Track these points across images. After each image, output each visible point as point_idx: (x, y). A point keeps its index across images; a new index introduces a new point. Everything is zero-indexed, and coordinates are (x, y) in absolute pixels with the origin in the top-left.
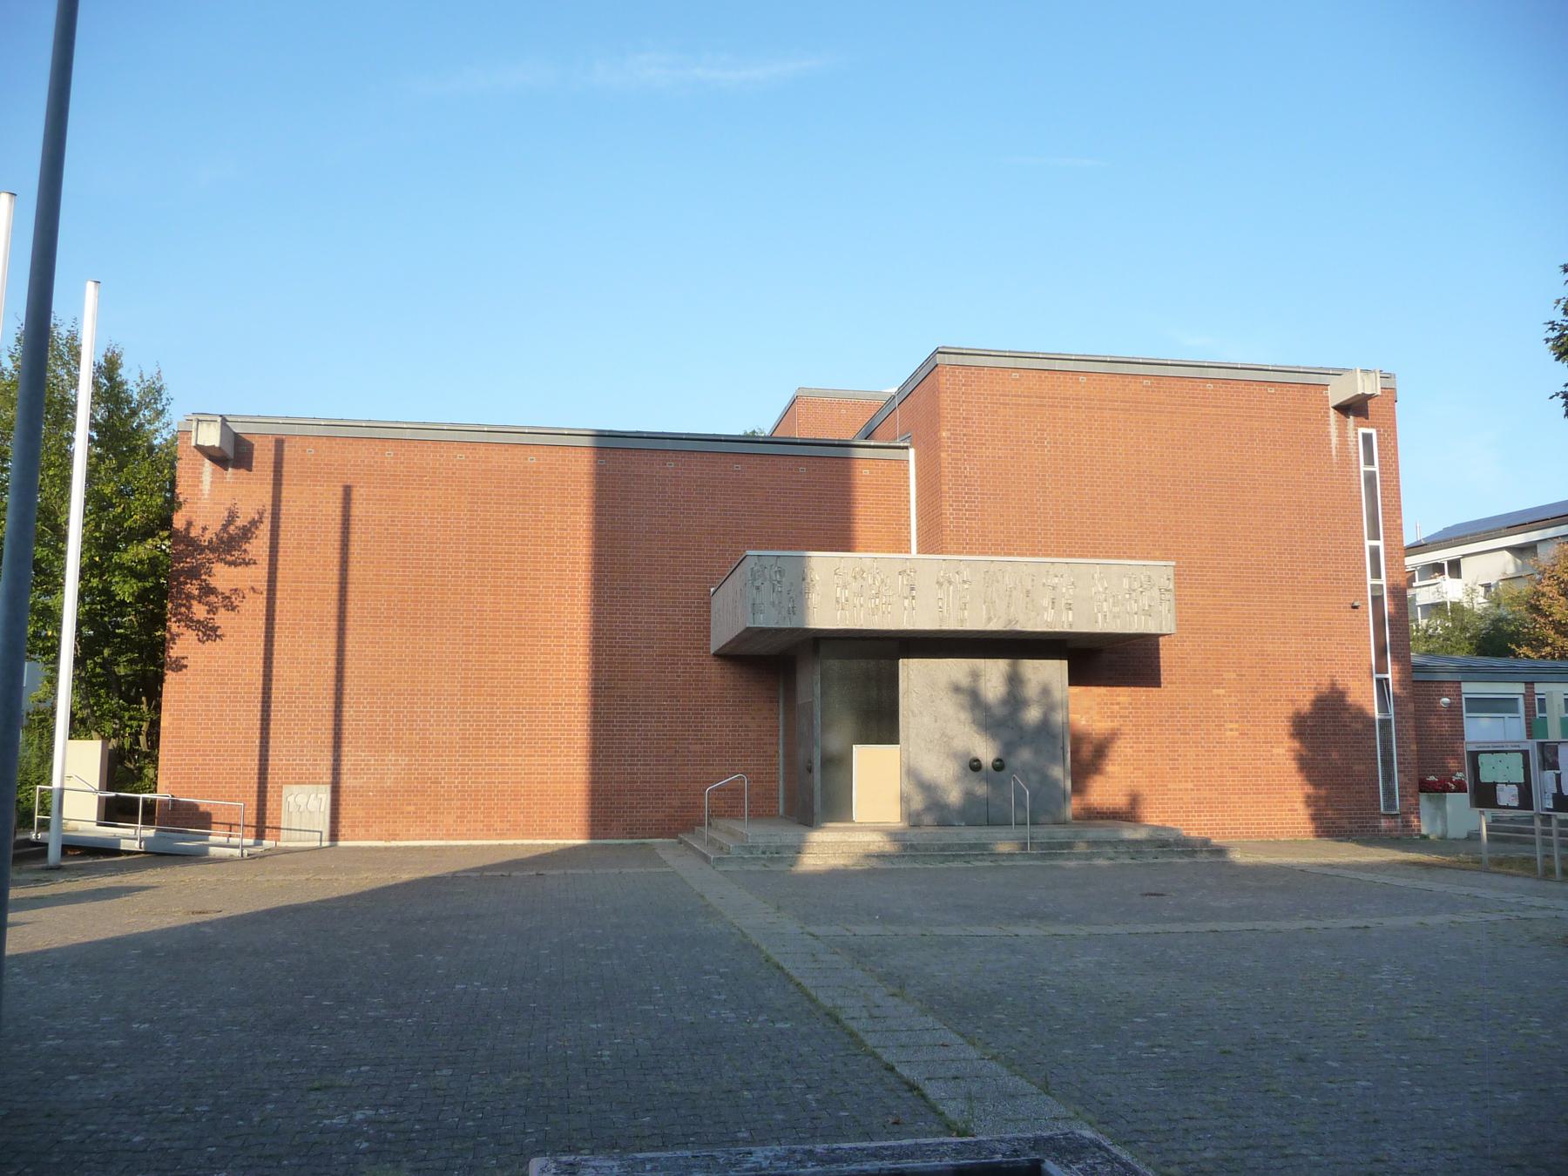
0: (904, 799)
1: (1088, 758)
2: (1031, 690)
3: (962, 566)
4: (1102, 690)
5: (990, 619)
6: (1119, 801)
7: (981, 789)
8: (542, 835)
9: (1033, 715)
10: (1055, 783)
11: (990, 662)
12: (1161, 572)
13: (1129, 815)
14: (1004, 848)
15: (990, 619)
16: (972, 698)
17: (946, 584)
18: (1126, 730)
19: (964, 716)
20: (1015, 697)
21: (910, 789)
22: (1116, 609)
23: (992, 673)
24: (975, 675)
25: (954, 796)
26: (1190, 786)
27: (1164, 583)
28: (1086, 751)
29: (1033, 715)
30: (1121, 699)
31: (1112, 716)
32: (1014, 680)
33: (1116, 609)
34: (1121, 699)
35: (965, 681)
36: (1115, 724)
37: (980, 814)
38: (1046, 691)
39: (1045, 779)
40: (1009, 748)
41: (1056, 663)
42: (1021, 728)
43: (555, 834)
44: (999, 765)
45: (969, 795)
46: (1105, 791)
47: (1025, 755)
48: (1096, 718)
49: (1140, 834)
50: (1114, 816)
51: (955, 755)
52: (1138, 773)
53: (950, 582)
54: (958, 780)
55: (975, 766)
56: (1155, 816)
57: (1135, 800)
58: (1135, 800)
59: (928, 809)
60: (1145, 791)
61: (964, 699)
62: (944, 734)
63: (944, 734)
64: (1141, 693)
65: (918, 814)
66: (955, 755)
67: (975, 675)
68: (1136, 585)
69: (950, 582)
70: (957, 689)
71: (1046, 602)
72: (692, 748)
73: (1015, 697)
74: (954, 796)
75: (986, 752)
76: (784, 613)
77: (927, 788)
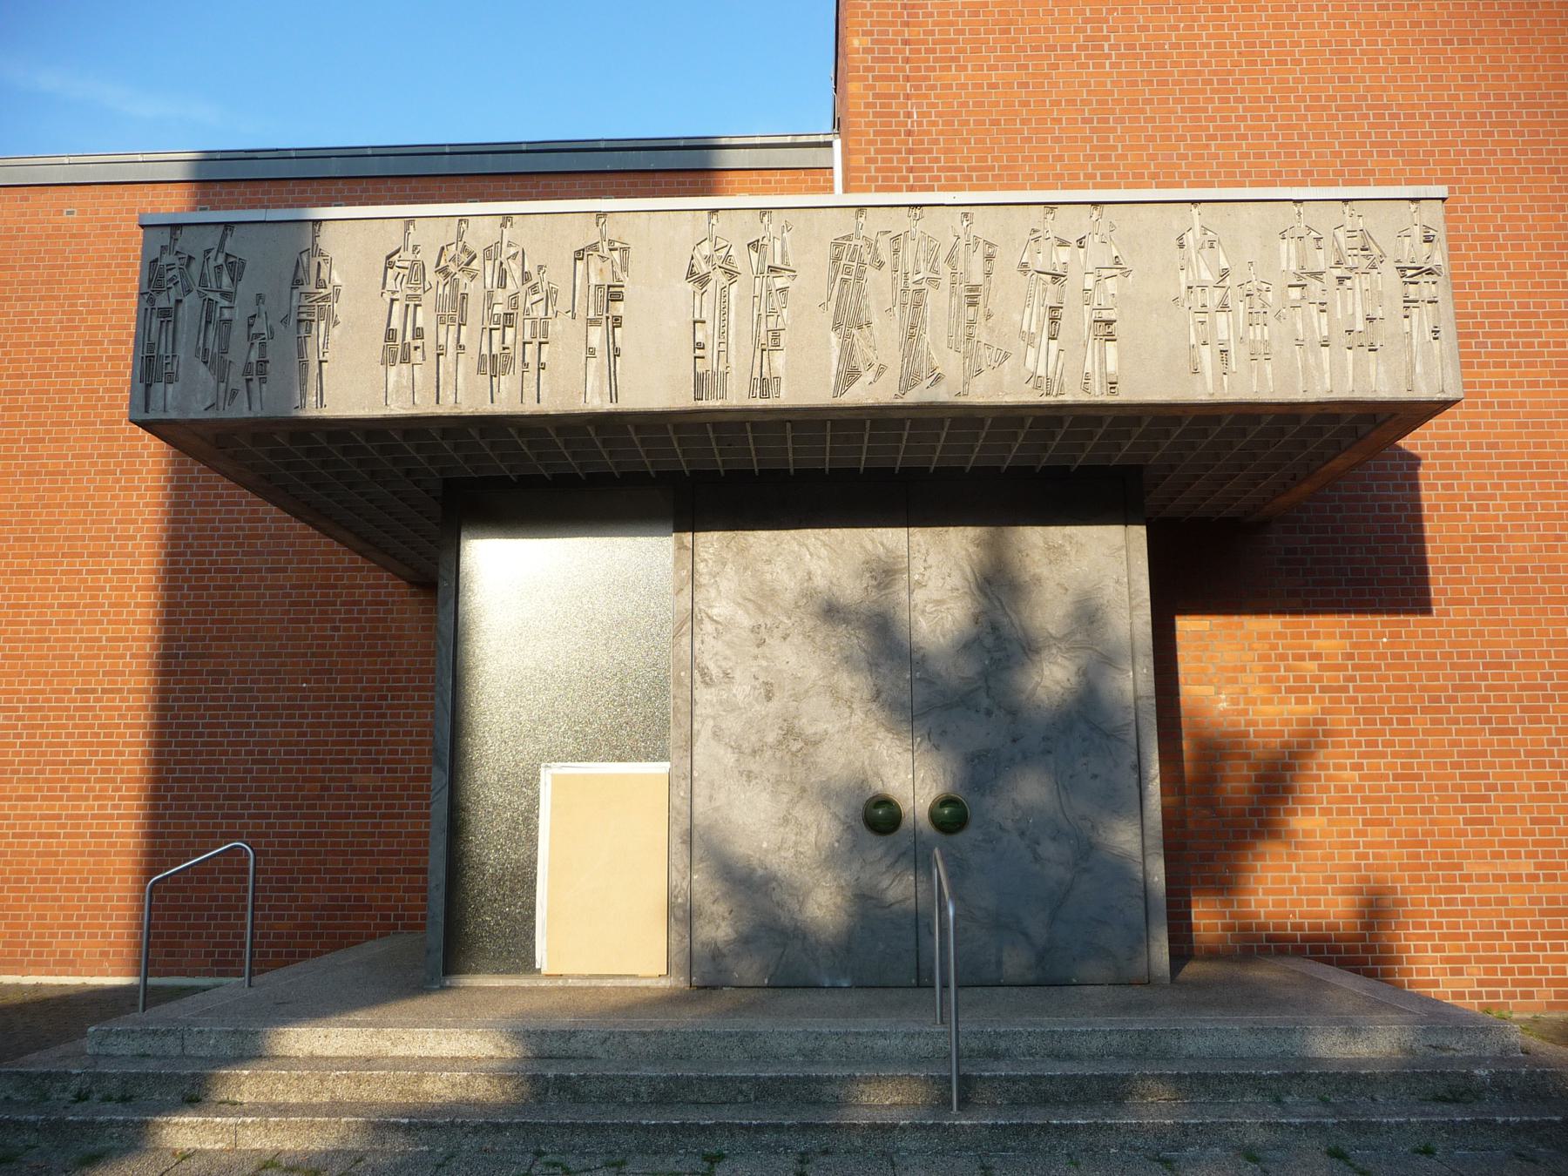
0: (682, 915)
1: (1226, 804)
2: (1048, 612)
3: (774, 224)
4: (1272, 624)
5: (851, 375)
6: (1333, 909)
7: (899, 888)
8: (38, 965)
9: (1052, 677)
10: (1118, 871)
11: (921, 537)
12: (1404, 221)
13: (1359, 952)
14: (884, 1100)
15: (851, 375)
16: (879, 638)
17: (718, 278)
18: (1341, 721)
19: (853, 683)
20: (998, 639)
21: (703, 884)
22: (1256, 333)
23: (931, 571)
24: (885, 574)
25: (823, 905)
26: (1526, 867)
27: (1415, 251)
28: (1237, 782)
29: (1052, 677)
30: (1319, 644)
31: (1300, 690)
32: (997, 585)
33: (1256, 333)
34: (1319, 644)
35: (852, 590)
36: (1310, 709)
37: (878, 959)
38: (1088, 615)
39: (1086, 852)
40: (982, 771)
41: (1112, 534)
42: (1013, 713)
43: (66, 963)
44: (951, 817)
45: (865, 902)
46: (1295, 881)
47: (1031, 790)
48: (1257, 692)
49: (1377, 1044)
50: (1320, 948)
51: (827, 794)
52: (1380, 834)
53: (731, 274)
54: (831, 860)
55: (880, 817)
56: (1443, 965)
57: (1376, 910)
58: (1376, 910)
59: (746, 941)
60: (1400, 881)
61: (855, 640)
62: (790, 732)
63: (790, 732)
64: (1377, 629)
65: (716, 955)
66: (827, 794)
67: (885, 574)
68: (1321, 260)
69: (731, 274)
70: (831, 612)
71: (1034, 319)
72: (359, 779)
73: (998, 639)
74: (823, 905)
75: (914, 780)
76: (236, 379)
77: (745, 883)
